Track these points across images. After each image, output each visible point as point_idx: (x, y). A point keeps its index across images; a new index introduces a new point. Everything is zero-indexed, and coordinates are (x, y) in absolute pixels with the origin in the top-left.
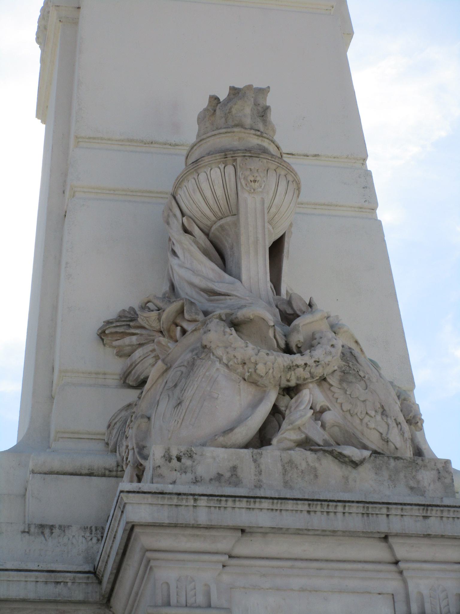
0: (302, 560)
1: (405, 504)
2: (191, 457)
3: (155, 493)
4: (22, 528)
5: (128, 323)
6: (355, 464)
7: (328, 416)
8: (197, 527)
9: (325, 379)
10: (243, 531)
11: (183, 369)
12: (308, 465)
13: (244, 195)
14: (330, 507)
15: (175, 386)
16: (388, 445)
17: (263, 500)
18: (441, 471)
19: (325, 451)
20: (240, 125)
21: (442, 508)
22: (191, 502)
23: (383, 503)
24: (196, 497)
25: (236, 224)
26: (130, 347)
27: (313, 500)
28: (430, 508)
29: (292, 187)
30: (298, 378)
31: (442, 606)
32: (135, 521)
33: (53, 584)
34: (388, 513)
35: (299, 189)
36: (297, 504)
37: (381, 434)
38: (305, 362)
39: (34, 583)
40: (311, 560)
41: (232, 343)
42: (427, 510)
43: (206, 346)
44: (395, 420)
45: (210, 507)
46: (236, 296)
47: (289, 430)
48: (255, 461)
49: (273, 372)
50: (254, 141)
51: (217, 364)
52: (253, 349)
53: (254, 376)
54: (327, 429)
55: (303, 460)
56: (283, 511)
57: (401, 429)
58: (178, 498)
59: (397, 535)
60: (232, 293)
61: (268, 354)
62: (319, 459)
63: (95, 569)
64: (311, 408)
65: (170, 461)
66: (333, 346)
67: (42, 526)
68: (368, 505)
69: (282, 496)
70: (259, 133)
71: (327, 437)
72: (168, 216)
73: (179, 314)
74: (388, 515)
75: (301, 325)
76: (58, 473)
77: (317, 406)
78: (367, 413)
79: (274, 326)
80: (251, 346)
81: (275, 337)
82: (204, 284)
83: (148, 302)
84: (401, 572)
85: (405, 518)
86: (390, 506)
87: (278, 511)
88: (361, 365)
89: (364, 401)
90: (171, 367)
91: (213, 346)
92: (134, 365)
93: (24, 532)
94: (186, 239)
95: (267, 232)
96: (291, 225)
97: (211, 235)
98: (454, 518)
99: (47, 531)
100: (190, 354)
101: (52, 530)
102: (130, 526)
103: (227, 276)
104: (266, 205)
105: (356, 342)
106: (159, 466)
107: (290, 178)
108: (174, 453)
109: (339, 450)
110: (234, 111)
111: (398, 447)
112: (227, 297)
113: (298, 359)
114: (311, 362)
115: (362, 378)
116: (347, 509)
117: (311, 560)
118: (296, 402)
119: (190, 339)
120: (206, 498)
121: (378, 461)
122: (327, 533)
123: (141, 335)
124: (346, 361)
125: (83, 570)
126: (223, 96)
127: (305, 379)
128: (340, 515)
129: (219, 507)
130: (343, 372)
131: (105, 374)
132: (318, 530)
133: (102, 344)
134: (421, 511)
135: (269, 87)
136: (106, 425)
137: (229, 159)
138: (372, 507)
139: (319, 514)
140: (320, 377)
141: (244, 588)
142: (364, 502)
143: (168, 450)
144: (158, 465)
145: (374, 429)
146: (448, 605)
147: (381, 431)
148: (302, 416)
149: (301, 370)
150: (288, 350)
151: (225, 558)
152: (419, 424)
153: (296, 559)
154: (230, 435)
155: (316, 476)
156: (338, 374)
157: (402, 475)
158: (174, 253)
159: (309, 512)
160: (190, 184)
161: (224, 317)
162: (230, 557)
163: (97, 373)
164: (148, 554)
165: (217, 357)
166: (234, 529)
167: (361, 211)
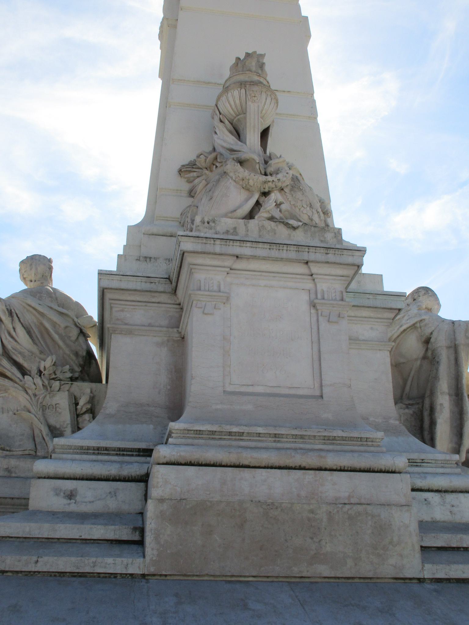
0: (266, 272)
1: (317, 247)
2: (214, 222)
3: (195, 237)
4: (136, 258)
5: (192, 166)
6: (294, 228)
7: (283, 207)
8: (215, 254)
9: (282, 189)
10: (237, 257)
11: (214, 183)
12: (272, 228)
13: (249, 103)
14: (280, 247)
15: (210, 191)
16: (312, 221)
17: (247, 242)
18: (336, 234)
19: (280, 222)
20: (250, 70)
21: (335, 250)
22: (212, 242)
23: (306, 246)
24: (215, 239)
25: (245, 118)
26: (193, 178)
27: (272, 243)
28: (329, 249)
29: (273, 101)
30: (269, 188)
31: (333, 296)
32: (184, 250)
33: (149, 283)
34: (308, 251)
35: (277, 103)
36: (264, 245)
37: (309, 216)
38: (273, 180)
39: (140, 282)
40: (270, 272)
41: (237, 170)
42: (328, 250)
43: (225, 172)
44: (317, 210)
45: (222, 244)
46: (243, 151)
47: (264, 212)
48: (245, 225)
49: (257, 184)
50: (256, 78)
51: (230, 180)
52: (248, 173)
53: (248, 186)
54: (282, 212)
55: (269, 225)
56: (257, 248)
57: (319, 215)
58: (206, 240)
59: (312, 262)
60: (242, 150)
61: (255, 175)
62: (277, 226)
63: (169, 276)
64: (275, 202)
65: (204, 224)
66: (287, 173)
67: (146, 257)
68: (299, 247)
69: (257, 241)
70: (258, 74)
71: (281, 215)
72: (213, 115)
73: (215, 160)
74: (308, 252)
75: (273, 163)
76: (156, 235)
77: (278, 201)
78: (302, 206)
79: (259, 163)
80: (246, 171)
81: (259, 169)
82: (228, 146)
83: (201, 154)
84: (314, 280)
85: (317, 254)
86: (310, 248)
87: (255, 248)
88: (301, 184)
89: (302, 200)
90: (209, 183)
91: (228, 171)
92: (195, 186)
93: (137, 260)
94: (221, 125)
95: (260, 122)
96: (273, 121)
97: (233, 124)
98: (341, 254)
99: (148, 260)
100: (218, 176)
101: (150, 259)
102: (182, 252)
103: (239, 143)
104: (260, 109)
105: (300, 174)
106: (198, 226)
107: (273, 97)
108: (206, 220)
109: (287, 222)
110: (247, 64)
111: (317, 223)
112: (239, 152)
113: (269, 178)
114: (275, 180)
115: (301, 190)
116: (288, 248)
117: (270, 272)
118: (268, 199)
119: (220, 170)
120: (219, 240)
121: (306, 228)
122: (279, 259)
123: (198, 172)
124: (294, 182)
125: (163, 277)
126: (242, 57)
127: (273, 188)
128: (285, 251)
129: (226, 245)
130: (292, 186)
131: (181, 190)
132: (274, 258)
133: (180, 176)
134: (325, 251)
135: (265, 54)
136: (180, 213)
137: (243, 86)
138: (301, 248)
139: (275, 250)
140: (280, 188)
141: (237, 284)
142: (297, 245)
143: (203, 219)
144: (198, 225)
145: (306, 214)
146: (336, 295)
147: (309, 215)
148: (270, 206)
149: (270, 183)
150: (266, 174)
151: (228, 269)
152: (329, 214)
153: (263, 272)
154: (234, 213)
155: (275, 233)
156: (289, 187)
157: (317, 234)
158: (216, 133)
159: (270, 249)
160: (224, 98)
161: (235, 159)
162: (231, 269)
163: (177, 190)
164: (191, 266)
165: (230, 177)
166: (233, 255)
167: (309, 119)
